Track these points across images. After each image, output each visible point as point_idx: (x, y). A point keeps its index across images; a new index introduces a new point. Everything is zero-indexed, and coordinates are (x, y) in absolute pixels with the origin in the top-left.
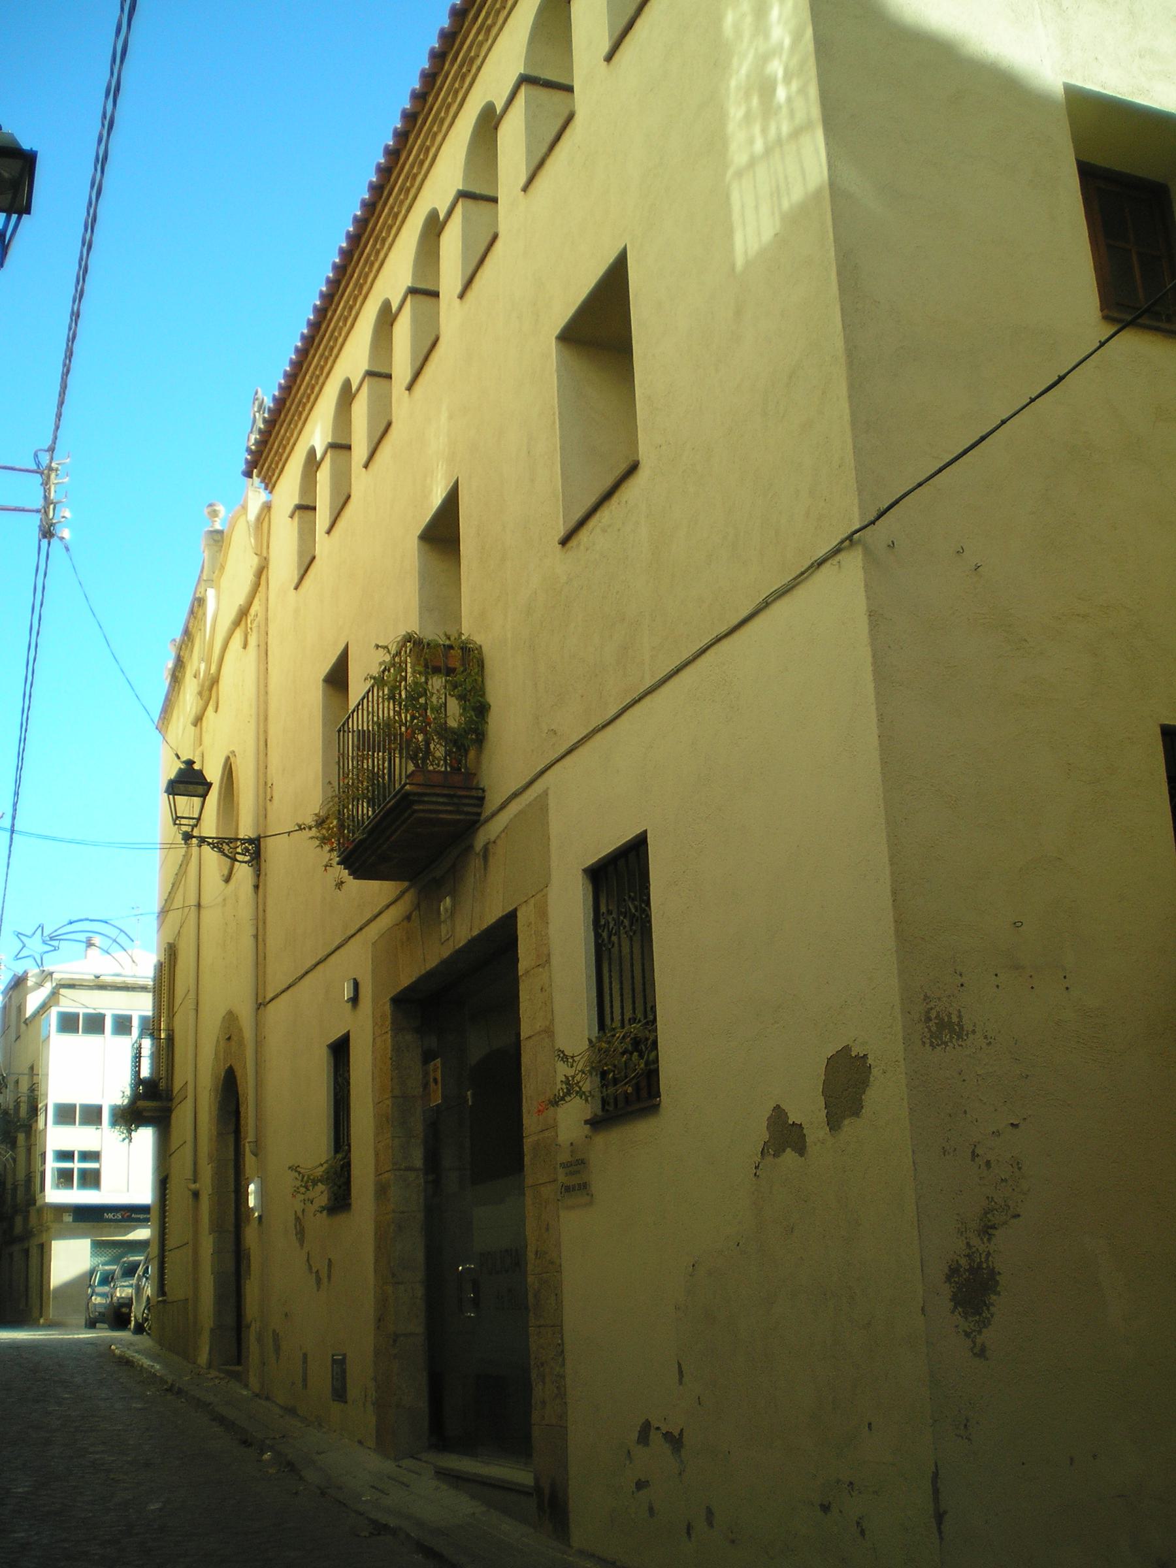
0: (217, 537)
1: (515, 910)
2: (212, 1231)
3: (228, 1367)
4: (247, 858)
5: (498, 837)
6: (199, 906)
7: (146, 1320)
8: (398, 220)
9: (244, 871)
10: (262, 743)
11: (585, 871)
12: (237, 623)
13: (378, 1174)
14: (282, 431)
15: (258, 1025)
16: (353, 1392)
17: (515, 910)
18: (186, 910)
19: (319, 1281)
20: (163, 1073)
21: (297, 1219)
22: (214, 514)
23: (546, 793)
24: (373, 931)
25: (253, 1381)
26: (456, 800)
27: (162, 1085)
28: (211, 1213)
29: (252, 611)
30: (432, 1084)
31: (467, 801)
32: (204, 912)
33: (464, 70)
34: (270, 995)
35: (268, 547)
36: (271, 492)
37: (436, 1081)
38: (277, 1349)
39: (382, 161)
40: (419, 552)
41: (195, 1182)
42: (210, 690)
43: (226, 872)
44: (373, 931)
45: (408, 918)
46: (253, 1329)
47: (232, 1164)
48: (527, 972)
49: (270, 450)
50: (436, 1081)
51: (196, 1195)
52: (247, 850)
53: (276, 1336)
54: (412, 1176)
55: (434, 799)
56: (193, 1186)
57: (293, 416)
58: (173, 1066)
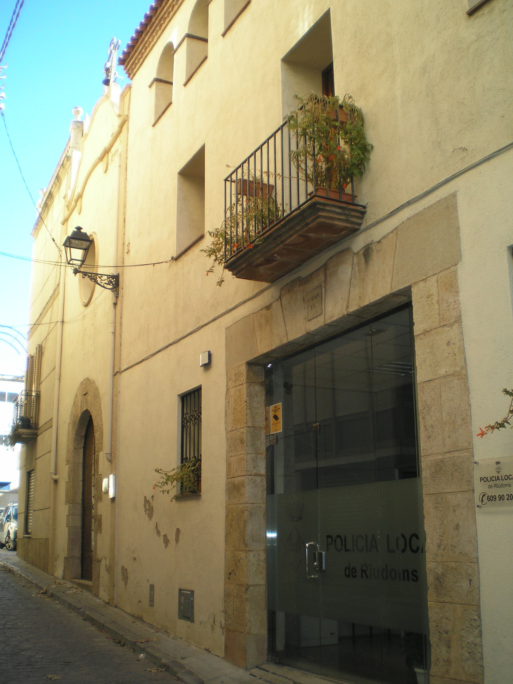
0: (79, 125)
1: (410, 287)
2: (67, 502)
3: (77, 580)
4: (111, 287)
5: (384, 237)
6: (63, 322)
7: (8, 542)
8: (148, 48)
9: (103, 295)
10: (121, 221)
11: (508, 247)
12: (101, 159)
13: (229, 475)
14: (147, 38)
15: (115, 386)
16: (199, 615)
17: (410, 287)
18: (52, 325)
19: (166, 541)
20: (33, 414)
21: (146, 501)
22: (77, 112)
23: (454, 195)
24: (228, 320)
25: (103, 594)
26: (347, 212)
27: (32, 421)
28: (67, 492)
29: (113, 150)
30: (272, 420)
31: (353, 213)
32: (65, 325)
33: (170, 10)
34: (122, 369)
35: (129, 109)
36: (132, 79)
37: (276, 418)
38: (125, 578)
39: (139, 28)
40: (282, 69)
41: (56, 474)
42: (77, 201)
43: (86, 302)
44: (228, 320)
45: (268, 307)
46: (103, 562)
47: (81, 465)
48: (426, 332)
49: (136, 51)
50: (276, 418)
51: (56, 482)
52: (111, 282)
53: (124, 571)
54: (258, 479)
55: (333, 209)
56: (55, 477)
57: (156, 27)
58: (39, 411)
